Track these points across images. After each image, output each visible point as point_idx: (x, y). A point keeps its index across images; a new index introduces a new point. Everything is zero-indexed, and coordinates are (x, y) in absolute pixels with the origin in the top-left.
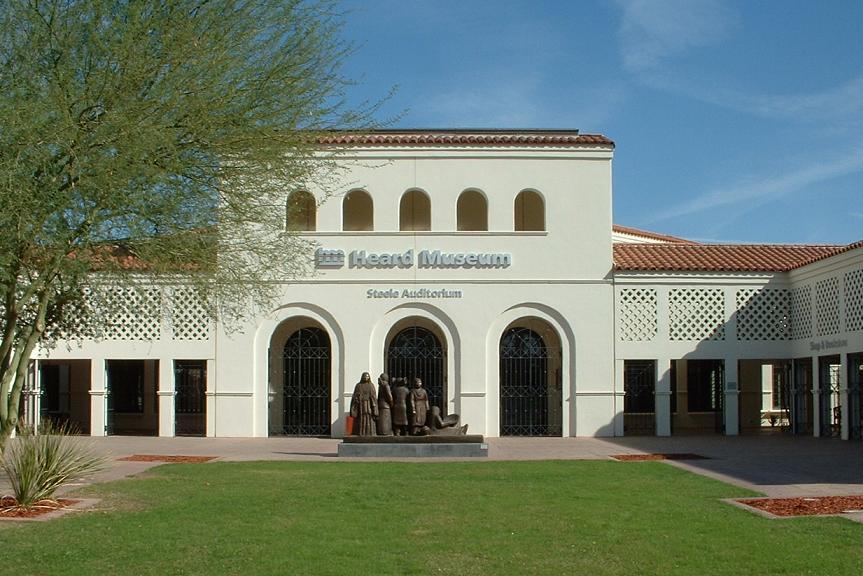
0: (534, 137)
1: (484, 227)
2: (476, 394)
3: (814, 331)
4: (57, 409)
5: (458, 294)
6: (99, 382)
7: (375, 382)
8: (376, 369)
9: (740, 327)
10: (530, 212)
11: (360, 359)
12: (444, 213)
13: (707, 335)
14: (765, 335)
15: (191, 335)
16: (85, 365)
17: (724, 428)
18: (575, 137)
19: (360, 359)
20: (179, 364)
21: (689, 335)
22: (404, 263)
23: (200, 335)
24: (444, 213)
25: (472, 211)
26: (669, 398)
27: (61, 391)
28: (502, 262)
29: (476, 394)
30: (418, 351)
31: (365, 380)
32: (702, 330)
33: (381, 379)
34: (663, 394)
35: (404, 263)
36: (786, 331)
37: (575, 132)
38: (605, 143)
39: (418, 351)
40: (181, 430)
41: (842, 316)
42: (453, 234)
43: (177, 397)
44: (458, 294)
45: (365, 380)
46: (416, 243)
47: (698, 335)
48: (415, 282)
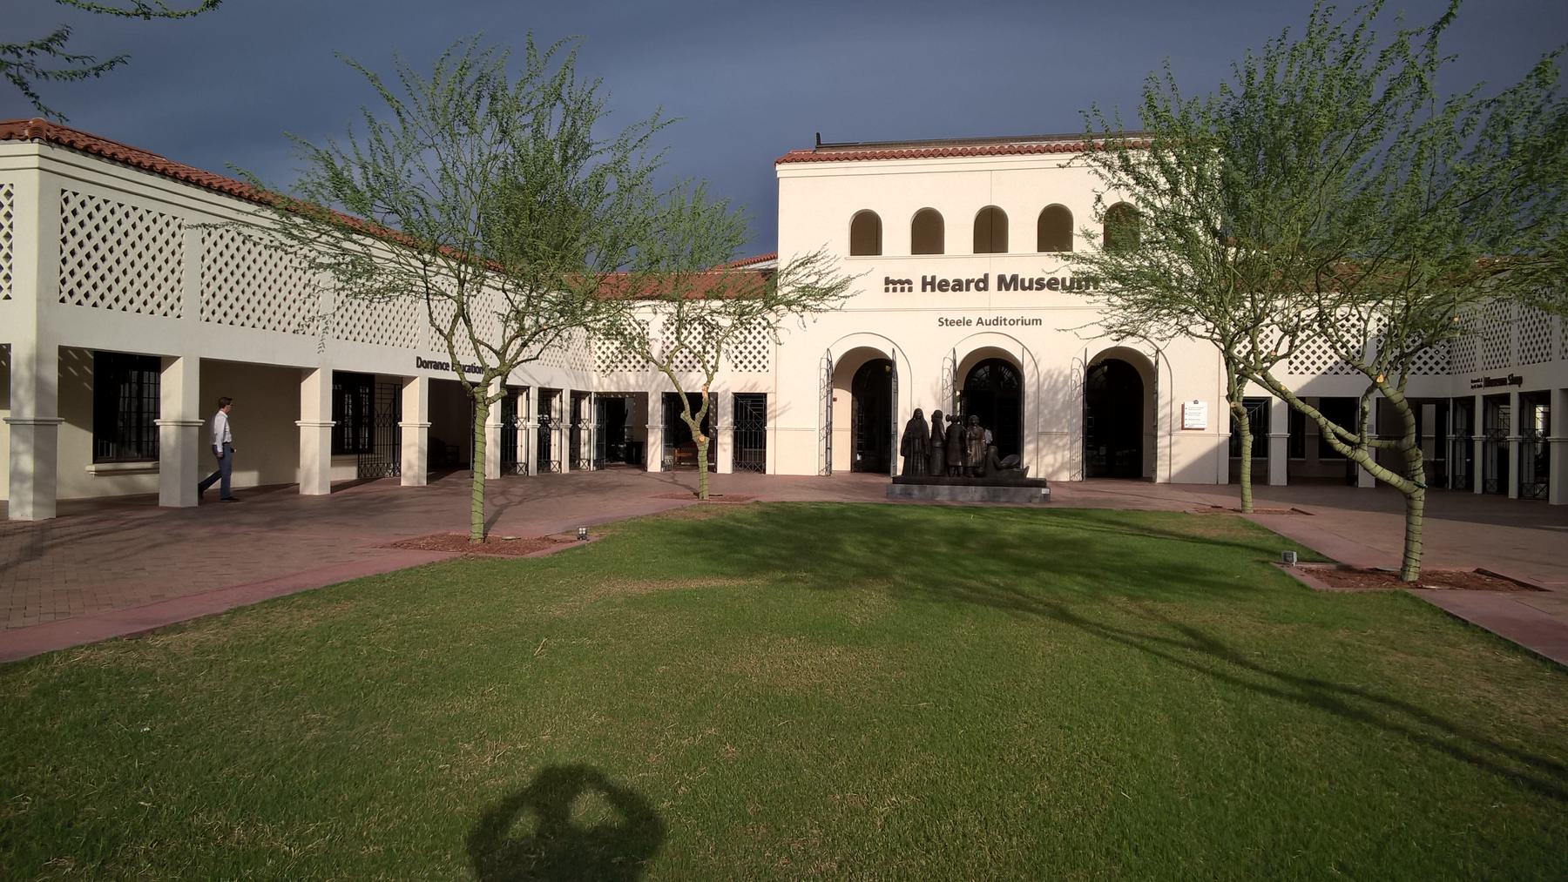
3: (1479, 364)
4: (433, 383)
6: (191, 299)
7: (928, 418)
9: (66, 274)
11: (923, 391)
13: (1324, 368)
14: (1426, 368)
15: (750, 367)
16: (642, 398)
17: (1356, 478)
19: (923, 391)
20: (740, 398)
21: (1302, 368)
22: (982, 284)
23: (759, 367)
24: (959, 233)
30: (991, 385)
31: (918, 414)
32: (1319, 363)
35: (982, 284)
36: (1443, 364)
40: (739, 461)
41: (1515, 346)
44: (1038, 321)
45: (918, 414)
47: (1313, 368)
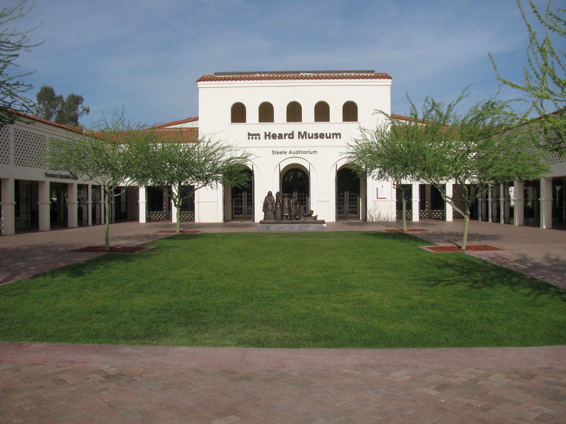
0: (316, 75)
1: (245, 122)
2: (323, 201)
5: (316, 152)
8: (275, 188)
10: (350, 112)
12: (308, 113)
18: (373, 75)
19: (266, 184)
22: (291, 136)
25: (322, 112)
26: (13, 207)
27: (122, 201)
28: (251, 137)
29: (323, 201)
30: (295, 181)
31: (270, 194)
33: (278, 194)
34: (143, 202)
35: (291, 136)
37: (373, 72)
38: (387, 77)
39: (295, 181)
42: (341, 123)
43: (397, 202)
44: (316, 152)
45: (270, 194)
46: (295, 127)
48: (294, 147)
